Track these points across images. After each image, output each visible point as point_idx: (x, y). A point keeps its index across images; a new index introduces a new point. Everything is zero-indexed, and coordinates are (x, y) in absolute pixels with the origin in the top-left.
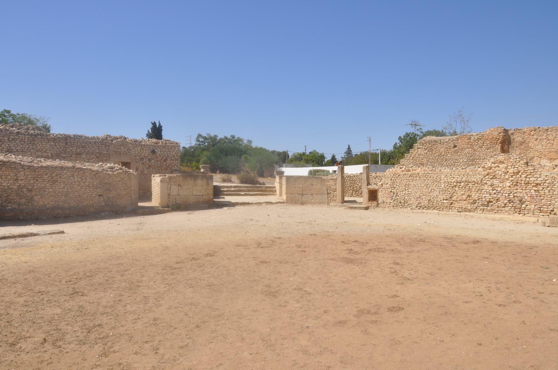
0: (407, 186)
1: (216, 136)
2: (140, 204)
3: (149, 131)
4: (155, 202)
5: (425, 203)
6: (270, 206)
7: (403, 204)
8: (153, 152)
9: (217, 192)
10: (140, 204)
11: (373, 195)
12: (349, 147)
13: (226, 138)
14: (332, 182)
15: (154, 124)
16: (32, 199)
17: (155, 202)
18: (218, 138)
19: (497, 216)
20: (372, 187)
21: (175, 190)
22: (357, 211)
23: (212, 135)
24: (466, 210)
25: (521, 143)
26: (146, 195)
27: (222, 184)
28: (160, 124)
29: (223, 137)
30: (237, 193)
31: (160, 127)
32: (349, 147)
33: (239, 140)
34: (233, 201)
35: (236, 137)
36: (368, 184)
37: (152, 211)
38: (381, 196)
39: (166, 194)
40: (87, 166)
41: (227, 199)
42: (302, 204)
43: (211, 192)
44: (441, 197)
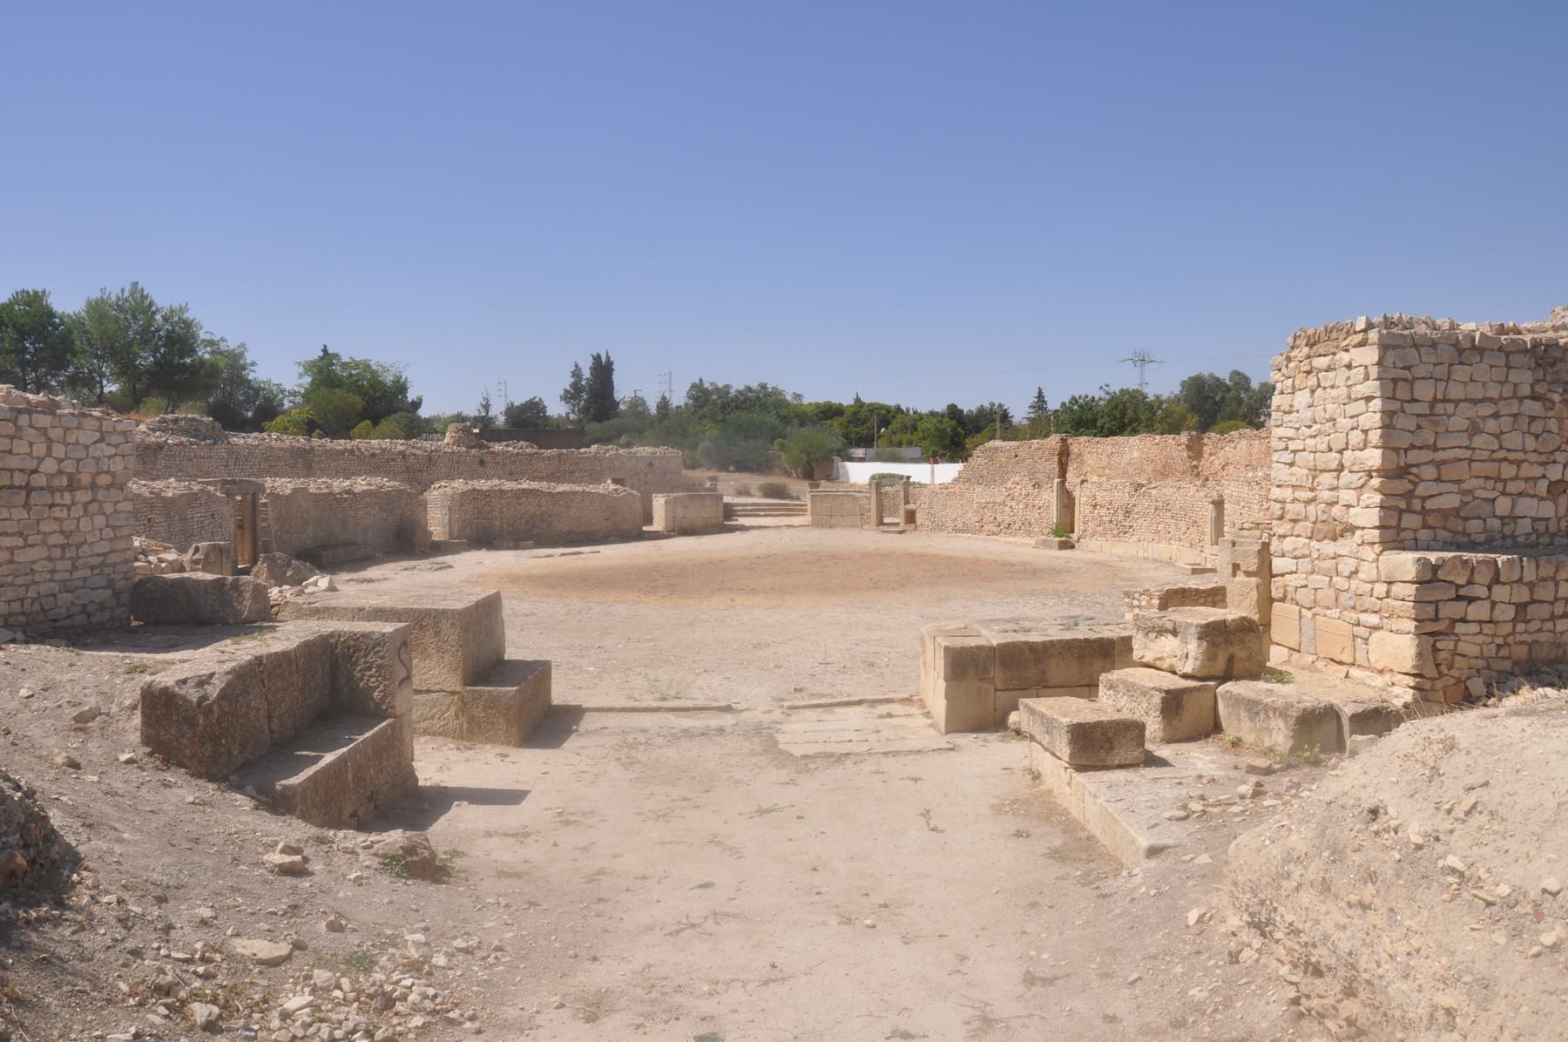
1: (727, 386)
3: (577, 374)
4: (658, 525)
5: (960, 526)
7: (939, 527)
8: (651, 465)
9: (729, 512)
11: (911, 517)
12: (1040, 392)
13: (749, 389)
14: (865, 501)
15: (597, 358)
18: (732, 391)
19: (1012, 539)
20: (911, 506)
23: (720, 385)
24: (994, 534)
25: (1079, 455)
26: (649, 519)
27: (737, 500)
29: (742, 388)
30: (755, 511)
31: (609, 364)
32: (1040, 392)
33: (777, 392)
35: (770, 386)
36: (907, 502)
37: (656, 536)
38: (919, 517)
41: (742, 521)
42: (831, 527)
43: (721, 513)
44: (975, 519)
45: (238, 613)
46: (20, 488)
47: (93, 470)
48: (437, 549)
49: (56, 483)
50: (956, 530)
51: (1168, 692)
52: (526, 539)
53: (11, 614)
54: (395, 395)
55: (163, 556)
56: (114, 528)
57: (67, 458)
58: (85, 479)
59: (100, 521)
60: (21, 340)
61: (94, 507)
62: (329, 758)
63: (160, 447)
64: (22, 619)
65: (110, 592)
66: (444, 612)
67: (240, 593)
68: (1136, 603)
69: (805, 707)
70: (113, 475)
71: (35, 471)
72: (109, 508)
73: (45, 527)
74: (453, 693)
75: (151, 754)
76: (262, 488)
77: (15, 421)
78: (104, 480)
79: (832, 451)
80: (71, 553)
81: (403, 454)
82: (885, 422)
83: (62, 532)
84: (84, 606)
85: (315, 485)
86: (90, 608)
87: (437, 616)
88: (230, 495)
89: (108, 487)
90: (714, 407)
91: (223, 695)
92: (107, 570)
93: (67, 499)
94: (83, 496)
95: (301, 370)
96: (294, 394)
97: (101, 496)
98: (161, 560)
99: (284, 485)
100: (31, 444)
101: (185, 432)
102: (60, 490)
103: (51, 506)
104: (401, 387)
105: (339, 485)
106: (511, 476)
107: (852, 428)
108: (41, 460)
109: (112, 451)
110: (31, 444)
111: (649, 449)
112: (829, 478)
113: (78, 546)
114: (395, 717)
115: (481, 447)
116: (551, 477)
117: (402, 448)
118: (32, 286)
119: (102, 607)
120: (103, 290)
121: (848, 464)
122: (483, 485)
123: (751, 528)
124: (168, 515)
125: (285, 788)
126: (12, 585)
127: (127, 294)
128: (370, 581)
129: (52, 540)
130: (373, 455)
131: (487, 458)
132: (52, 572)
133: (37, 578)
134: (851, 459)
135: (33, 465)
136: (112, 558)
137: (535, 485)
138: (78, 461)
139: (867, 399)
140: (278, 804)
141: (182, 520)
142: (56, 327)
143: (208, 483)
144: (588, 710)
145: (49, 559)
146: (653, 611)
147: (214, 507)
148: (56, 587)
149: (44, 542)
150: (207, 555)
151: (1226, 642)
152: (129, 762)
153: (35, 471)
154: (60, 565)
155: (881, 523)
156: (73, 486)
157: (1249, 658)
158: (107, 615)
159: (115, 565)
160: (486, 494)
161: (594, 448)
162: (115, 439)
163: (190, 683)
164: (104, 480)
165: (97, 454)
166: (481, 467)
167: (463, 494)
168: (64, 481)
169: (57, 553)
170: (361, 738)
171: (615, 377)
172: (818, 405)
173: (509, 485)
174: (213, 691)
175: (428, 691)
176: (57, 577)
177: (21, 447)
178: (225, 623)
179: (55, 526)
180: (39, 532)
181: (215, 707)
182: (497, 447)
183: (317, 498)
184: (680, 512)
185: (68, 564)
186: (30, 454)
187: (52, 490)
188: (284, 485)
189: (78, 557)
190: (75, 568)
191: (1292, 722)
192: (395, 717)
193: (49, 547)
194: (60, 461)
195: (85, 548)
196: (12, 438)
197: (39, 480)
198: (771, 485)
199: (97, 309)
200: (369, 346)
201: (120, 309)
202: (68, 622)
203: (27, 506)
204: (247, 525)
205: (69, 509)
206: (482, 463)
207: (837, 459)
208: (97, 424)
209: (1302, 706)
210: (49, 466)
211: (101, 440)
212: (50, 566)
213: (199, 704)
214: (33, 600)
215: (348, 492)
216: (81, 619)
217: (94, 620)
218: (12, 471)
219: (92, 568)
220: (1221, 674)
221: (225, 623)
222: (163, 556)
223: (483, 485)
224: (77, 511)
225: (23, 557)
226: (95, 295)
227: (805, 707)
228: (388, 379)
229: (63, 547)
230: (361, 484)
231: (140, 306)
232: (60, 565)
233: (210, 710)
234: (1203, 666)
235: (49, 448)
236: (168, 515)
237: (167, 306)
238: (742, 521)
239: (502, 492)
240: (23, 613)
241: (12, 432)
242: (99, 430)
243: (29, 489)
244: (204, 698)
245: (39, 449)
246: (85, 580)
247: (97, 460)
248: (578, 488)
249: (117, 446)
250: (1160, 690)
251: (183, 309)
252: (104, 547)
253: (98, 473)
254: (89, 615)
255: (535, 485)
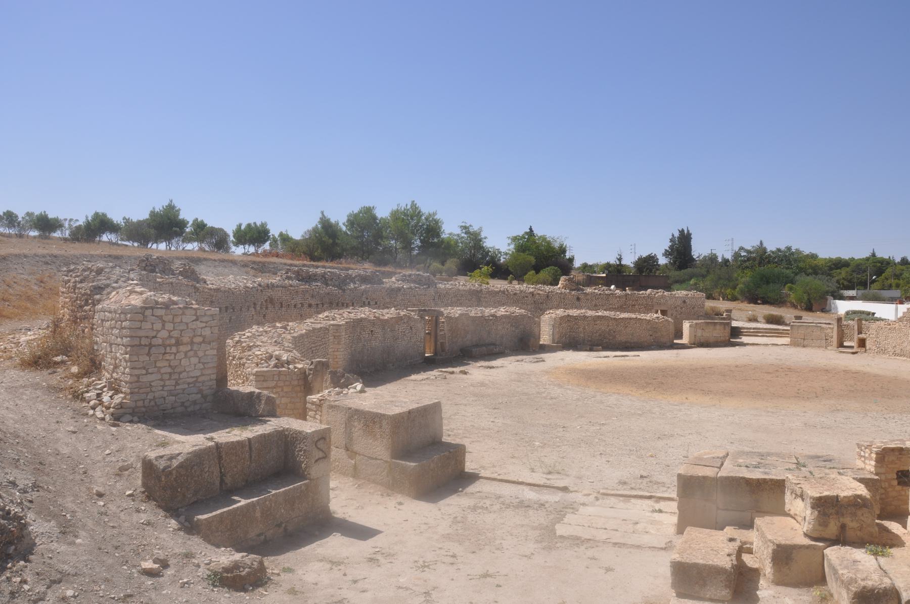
0: (887, 338)
2: (675, 341)
4: (685, 340)
6: (775, 348)
7: (882, 351)
8: (684, 302)
9: (736, 332)
10: (675, 341)
11: (862, 343)
13: (779, 250)
14: (829, 330)
15: (682, 232)
16: (615, 337)
17: (685, 340)
20: (862, 336)
21: (699, 333)
22: (844, 354)
26: (679, 335)
28: (688, 231)
29: (774, 249)
30: (756, 333)
34: (140, 429)
36: (860, 332)
39: (693, 334)
40: (642, 316)
45: (257, 411)
46: (145, 345)
47: (191, 335)
48: (544, 349)
49: (168, 342)
50: (895, 354)
51: (779, 546)
52: (598, 345)
53: (136, 407)
54: (560, 255)
55: (297, 365)
56: (204, 363)
57: (174, 329)
58: (186, 339)
59: (194, 360)
60: (362, 231)
61: (191, 353)
62: (243, 502)
63: (399, 289)
64: (144, 409)
65: (199, 396)
66: (384, 415)
67: (260, 401)
68: (862, 453)
69: (612, 495)
70: (204, 337)
71: (155, 337)
72: (200, 354)
73: (158, 364)
74: (386, 462)
75: (143, 492)
76: (442, 314)
77: (143, 314)
78: (198, 340)
79: (827, 292)
80: (176, 376)
81: (532, 293)
82: (879, 272)
83: (170, 366)
84: (183, 403)
85: (474, 312)
86: (186, 404)
87: (381, 417)
88: (422, 317)
89: (200, 343)
90: (759, 261)
91: (181, 466)
92: (198, 385)
93: (174, 350)
94: (183, 348)
95: (510, 241)
96: (506, 254)
97: (195, 348)
98: (295, 368)
99: (456, 311)
100: (153, 324)
101: (414, 282)
102: (170, 346)
103: (165, 353)
104: (563, 250)
105: (488, 311)
106: (596, 307)
107: (855, 275)
108: (158, 331)
109: (204, 325)
110: (153, 324)
111: (684, 292)
112: (823, 310)
113: (180, 373)
114: (310, 479)
115: (578, 290)
116: (622, 309)
117: (531, 290)
118: (368, 204)
119: (195, 403)
120: (398, 205)
121: (837, 301)
122: (574, 312)
123: (748, 344)
124: (383, 329)
125: (198, 520)
126: (138, 393)
127: (409, 207)
128: (493, 367)
129: (163, 371)
130: (515, 294)
131: (582, 297)
132: (163, 386)
133: (153, 389)
134: (842, 298)
135: (154, 334)
136: (200, 379)
137: (606, 313)
138: (181, 331)
139: (879, 255)
140: (190, 528)
141: (392, 331)
142: (377, 225)
143: (413, 311)
144: (482, 478)
145: (161, 380)
146: (626, 400)
147: (412, 324)
148: (165, 394)
149: (159, 371)
150: (316, 366)
151: (837, 513)
152: (129, 495)
153: (155, 337)
154: (167, 383)
155: (841, 345)
156: (178, 343)
157: (861, 529)
158: (198, 407)
159: (204, 382)
160: (576, 318)
161: (649, 290)
162: (205, 319)
163: (165, 458)
164: (198, 340)
165: (194, 327)
166: (578, 302)
167: (562, 318)
168: (173, 341)
169: (167, 377)
170: (274, 492)
171: (693, 243)
172: (830, 260)
173: (590, 313)
174: (175, 463)
175: (376, 459)
176: (166, 388)
177: (147, 325)
178: (250, 416)
179: (166, 364)
180: (156, 367)
181: (174, 472)
182: (589, 290)
183: (474, 319)
184: (699, 333)
185: (173, 382)
186: (152, 329)
187: (165, 346)
188: (456, 311)
189: (180, 379)
190: (177, 384)
191: (851, 595)
192: (310, 479)
193: (162, 374)
194: (170, 332)
195: (184, 374)
196: (141, 322)
197: (155, 342)
198: (772, 315)
199: (395, 215)
200: (550, 230)
201: (406, 215)
202: (172, 411)
203: (149, 354)
204: (433, 334)
205: (175, 354)
206: (578, 299)
207: (830, 298)
208: (193, 312)
209: (863, 584)
210: (164, 334)
211: (197, 320)
212: (162, 383)
213: (165, 468)
214: (150, 400)
215: (493, 316)
216: (180, 409)
217: (189, 410)
218: (140, 338)
219: (189, 384)
220: (834, 538)
221: (250, 416)
222: (297, 365)
223: (574, 312)
224: (181, 356)
225: (144, 379)
226: (395, 208)
227: (612, 495)
228: (556, 245)
229: (170, 374)
230: (502, 311)
231: (415, 213)
232: (167, 383)
233: (170, 473)
234: (814, 530)
235: (163, 325)
236: (383, 329)
237: (427, 214)
238: (745, 339)
239: (585, 317)
240: (144, 407)
241: (142, 319)
242: (196, 315)
243: (151, 346)
244: (169, 467)
245: (158, 326)
246: (184, 390)
247: (194, 330)
248: (633, 316)
249: (206, 322)
250: (773, 543)
251: (435, 214)
252: (198, 373)
253: (195, 336)
254: (186, 407)
255: (606, 313)
